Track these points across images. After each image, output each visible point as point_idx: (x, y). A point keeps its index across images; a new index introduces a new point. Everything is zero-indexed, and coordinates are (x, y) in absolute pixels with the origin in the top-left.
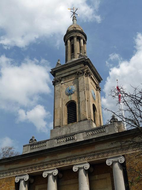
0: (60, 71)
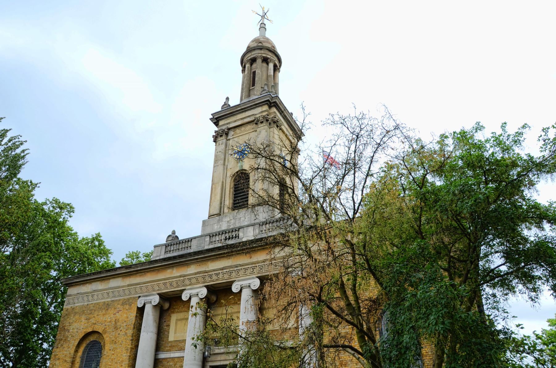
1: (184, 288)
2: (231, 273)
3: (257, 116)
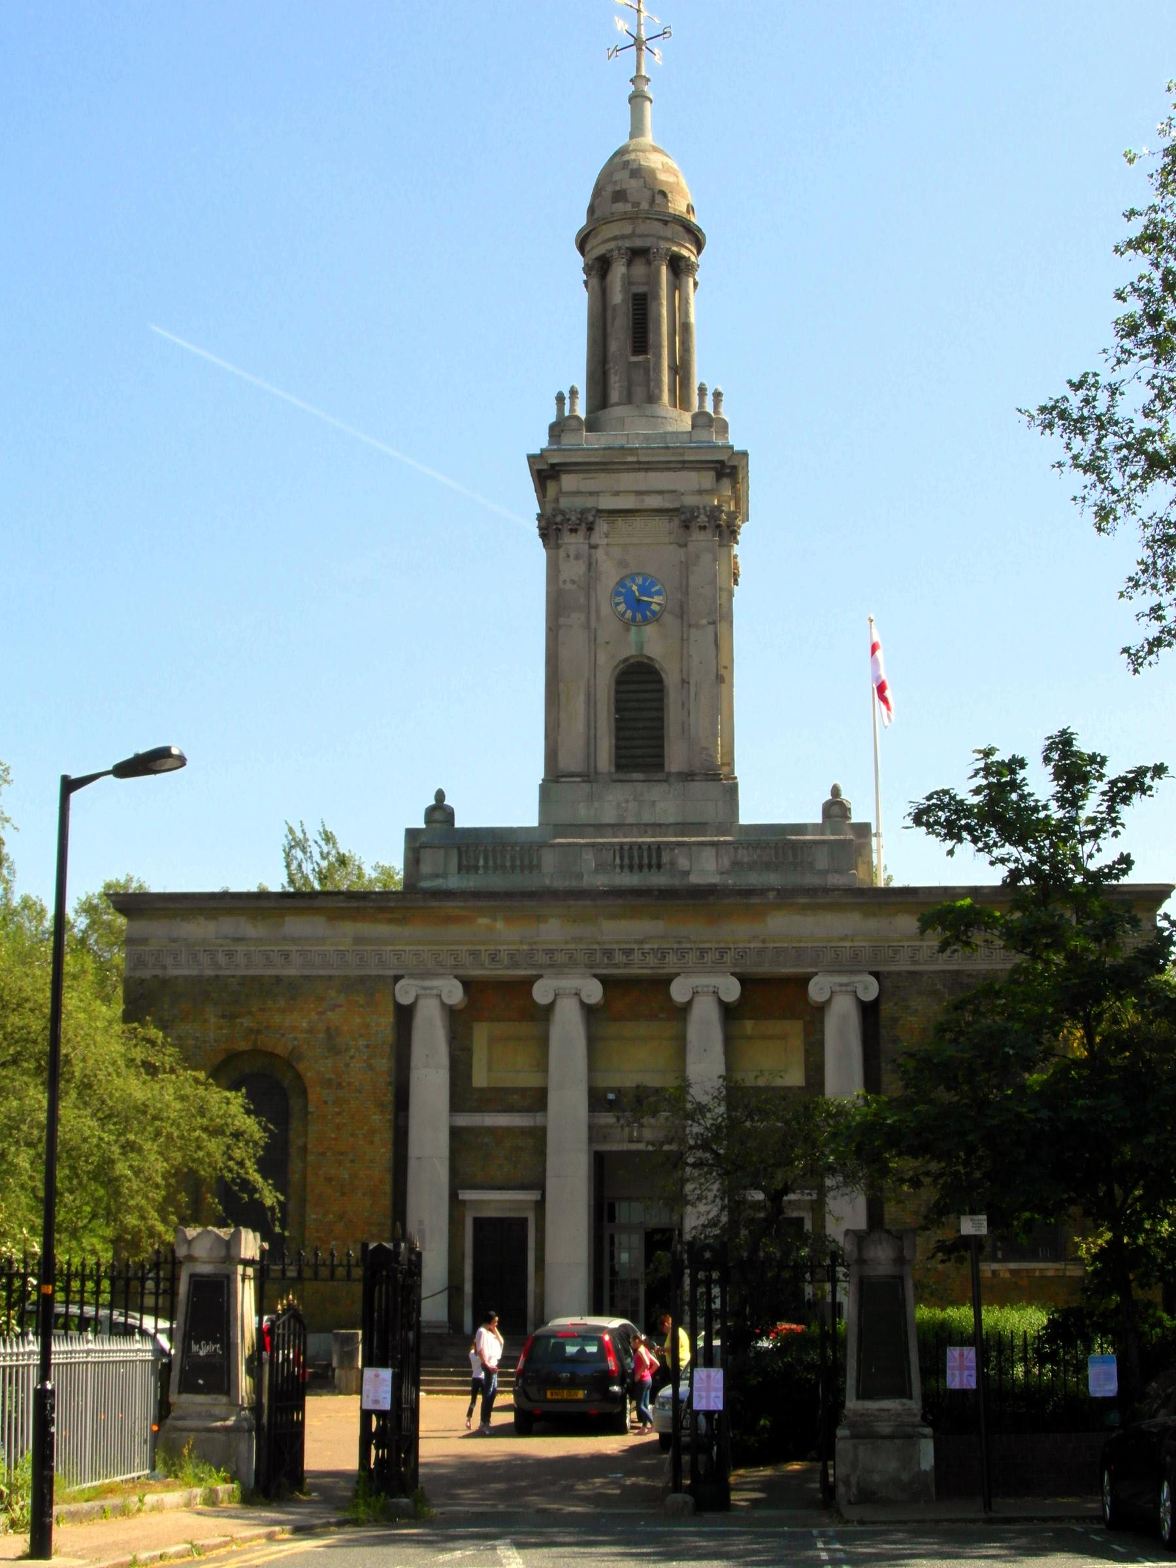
1: (810, 970)
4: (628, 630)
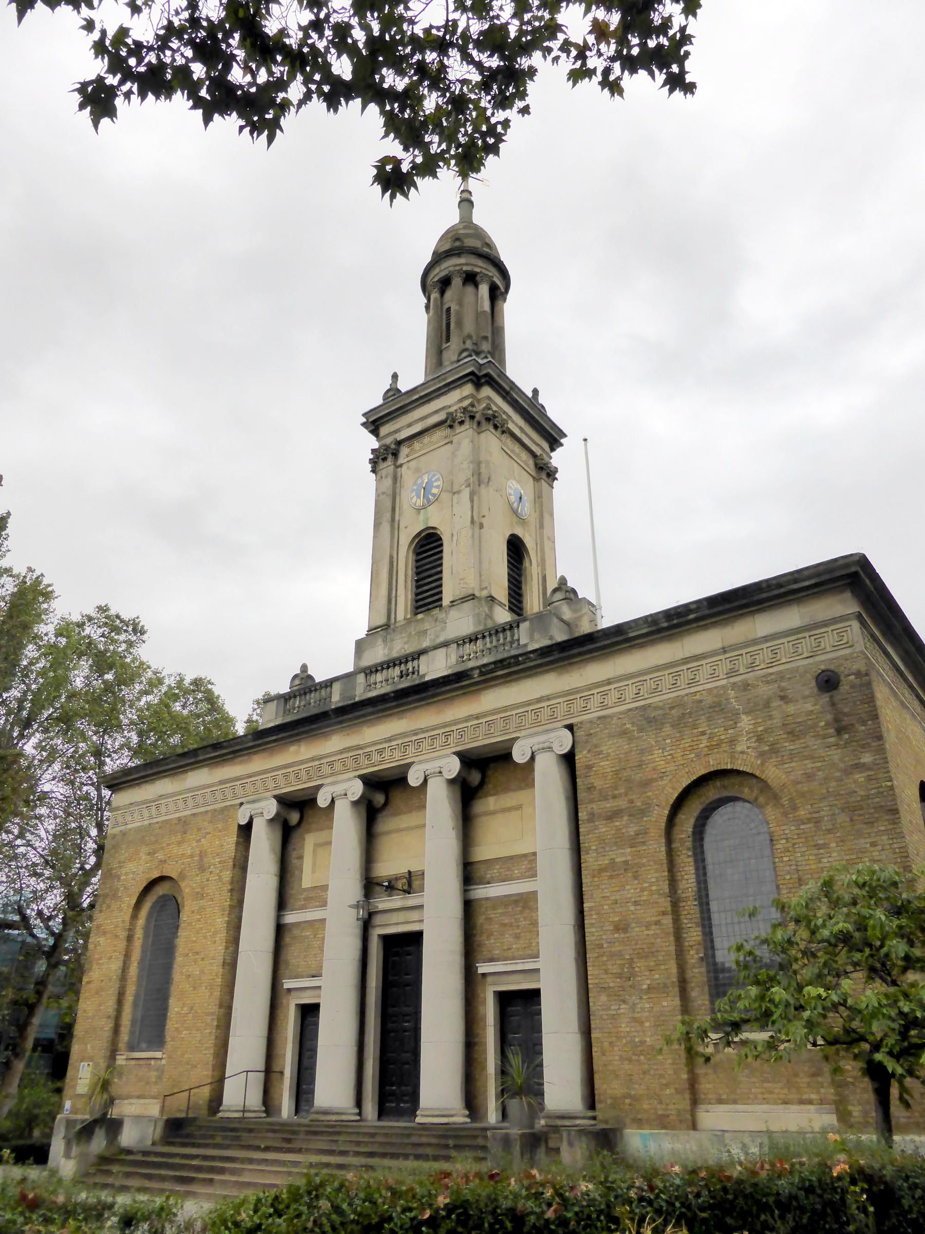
0: (392, 419)
1: (514, 735)
2: (406, 746)
3: (452, 410)
4: (419, 513)
